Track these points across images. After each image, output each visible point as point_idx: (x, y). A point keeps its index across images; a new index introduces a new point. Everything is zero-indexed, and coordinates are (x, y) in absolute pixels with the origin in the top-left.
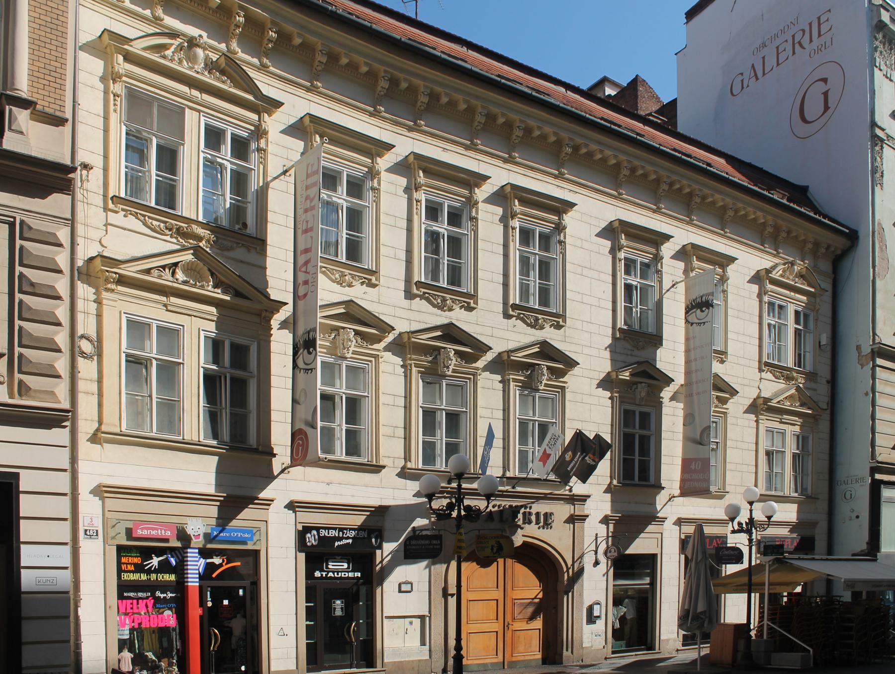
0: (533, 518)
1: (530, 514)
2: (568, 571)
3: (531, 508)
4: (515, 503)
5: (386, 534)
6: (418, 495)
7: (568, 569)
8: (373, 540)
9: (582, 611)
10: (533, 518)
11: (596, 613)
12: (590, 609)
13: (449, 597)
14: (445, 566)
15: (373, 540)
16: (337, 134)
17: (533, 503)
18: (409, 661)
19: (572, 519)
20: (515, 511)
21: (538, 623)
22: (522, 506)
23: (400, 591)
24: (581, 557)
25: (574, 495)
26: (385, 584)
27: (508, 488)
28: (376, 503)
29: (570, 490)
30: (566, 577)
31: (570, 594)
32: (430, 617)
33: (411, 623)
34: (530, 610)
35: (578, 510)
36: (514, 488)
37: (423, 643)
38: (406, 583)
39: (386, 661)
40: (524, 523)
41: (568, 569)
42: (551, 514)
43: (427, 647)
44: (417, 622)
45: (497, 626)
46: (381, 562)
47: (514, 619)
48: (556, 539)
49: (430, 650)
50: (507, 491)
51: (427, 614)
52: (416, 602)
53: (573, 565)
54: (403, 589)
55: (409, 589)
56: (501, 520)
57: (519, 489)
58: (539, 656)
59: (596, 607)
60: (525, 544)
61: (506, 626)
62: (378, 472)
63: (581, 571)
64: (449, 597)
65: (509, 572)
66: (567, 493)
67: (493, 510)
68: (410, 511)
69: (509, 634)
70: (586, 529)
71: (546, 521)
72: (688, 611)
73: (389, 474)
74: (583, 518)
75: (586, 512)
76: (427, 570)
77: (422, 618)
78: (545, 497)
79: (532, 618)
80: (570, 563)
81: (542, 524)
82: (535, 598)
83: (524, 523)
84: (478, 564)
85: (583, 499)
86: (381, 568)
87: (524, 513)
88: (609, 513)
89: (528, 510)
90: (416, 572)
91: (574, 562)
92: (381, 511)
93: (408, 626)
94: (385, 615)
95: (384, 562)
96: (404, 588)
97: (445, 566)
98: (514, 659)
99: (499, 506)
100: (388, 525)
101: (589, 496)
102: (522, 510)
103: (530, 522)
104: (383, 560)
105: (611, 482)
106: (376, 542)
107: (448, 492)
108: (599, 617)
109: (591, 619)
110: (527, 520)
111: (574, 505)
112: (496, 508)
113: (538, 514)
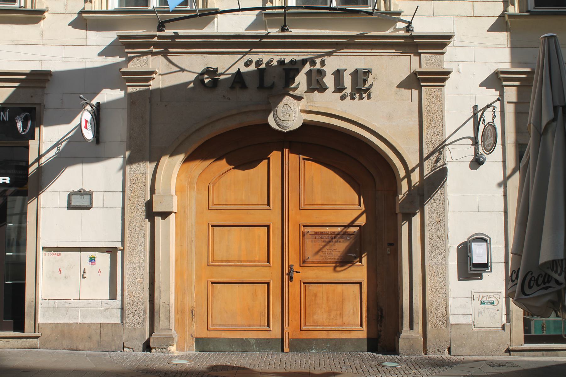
0: (329, 81)
1: (321, 73)
2: (408, 176)
3: (323, 63)
4: (289, 56)
5: (47, 115)
6: (105, 53)
7: (408, 173)
8: (20, 125)
9: (445, 253)
10: (329, 81)
11: (478, 257)
12: (464, 251)
13: (158, 219)
14: (151, 167)
15: (20, 125)
16: (560, 10)
17: (329, 54)
18: (82, 325)
19: (416, 81)
20: (290, 71)
21: (359, 272)
22: (304, 62)
23: (70, 207)
24: (440, 149)
25: (412, 37)
26: (43, 197)
27: (274, 31)
28: (27, 67)
29: (409, 28)
30: (404, 187)
31: (416, 220)
32: (123, 251)
33: (93, 260)
34: (341, 247)
35: (428, 62)
36: (283, 30)
37: (113, 297)
38: (81, 193)
39: (40, 320)
40: (310, 89)
41: (408, 173)
42: (367, 72)
43: (118, 302)
44: (104, 259)
45: (272, 274)
46: (37, 160)
47: (304, 262)
48: (384, 116)
49: (122, 309)
50: (267, 36)
51: (119, 246)
52: (101, 225)
53: (421, 165)
54: (73, 204)
55: (87, 204)
56: (261, 86)
57: (294, 31)
58: (362, 334)
59: (476, 246)
60: (306, 126)
61: (288, 274)
62: (36, 21)
63: (439, 178)
64: (158, 219)
65: (291, 176)
66: (402, 33)
67: (244, 69)
68: (88, 81)
69: (292, 289)
70: (446, 98)
71: (361, 85)
72: (516, 272)
73: (56, 25)
74: (440, 78)
75: (446, 67)
76: (121, 172)
77: (112, 251)
78: (350, 43)
79: (345, 261)
80: (413, 160)
81: (348, 91)
82: (351, 225)
83: (310, 89)
84: (229, 163)
85: (439, 42)
86: (39, 168)
87: (309, 74)
88: (507, 66)
89: (318, 66)
90: (102, 177)
91: (422, 160)
92: (38, 80)
93: (86, 265)
94: (41, 245)
95: (43, 161)
96: (84, 201)
97: (154, 164)
98: (304, 336)
99: (258, 63)
100: (52, 98)
101: (449, 37)
102: (307, 67)
103: (322, 88)
104: (40, 157)
105: (505, 10)
106: (24, 127)
107: (156, 45)
108: (485, 266)
109: (471, 270)
110: (316, 84)
111: (419, 55)
112: (253, 67)
113: (338, 74)
